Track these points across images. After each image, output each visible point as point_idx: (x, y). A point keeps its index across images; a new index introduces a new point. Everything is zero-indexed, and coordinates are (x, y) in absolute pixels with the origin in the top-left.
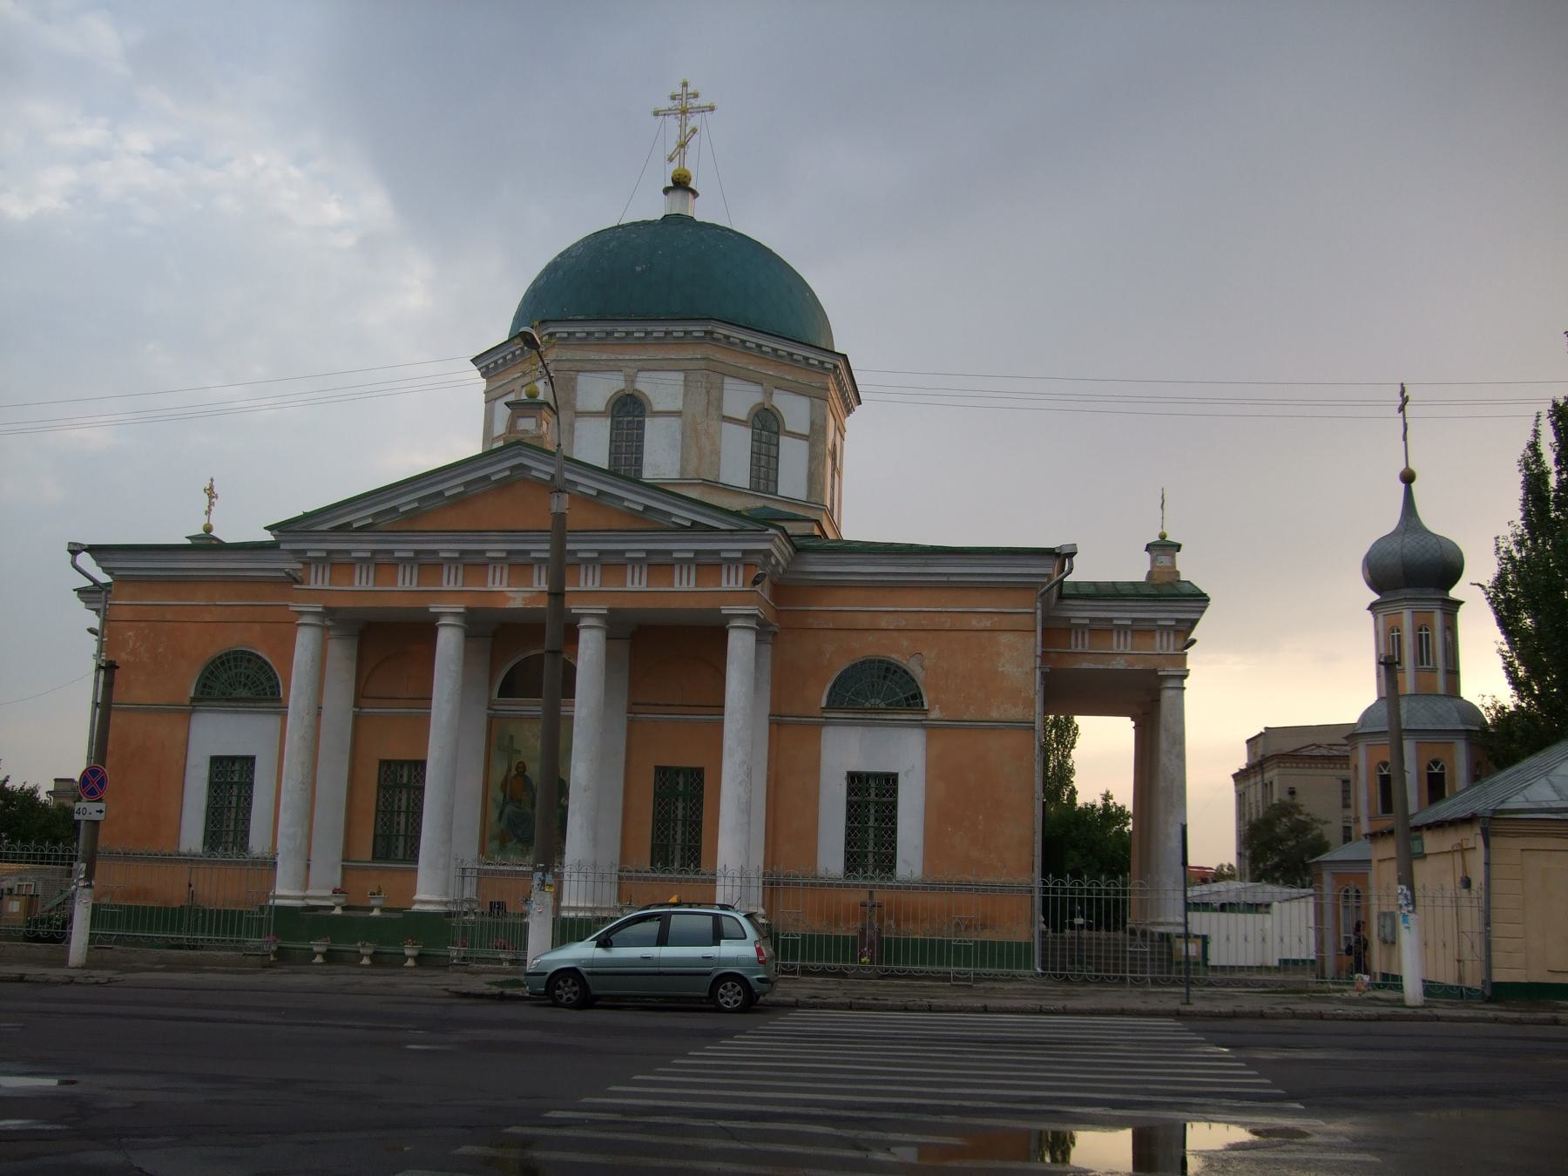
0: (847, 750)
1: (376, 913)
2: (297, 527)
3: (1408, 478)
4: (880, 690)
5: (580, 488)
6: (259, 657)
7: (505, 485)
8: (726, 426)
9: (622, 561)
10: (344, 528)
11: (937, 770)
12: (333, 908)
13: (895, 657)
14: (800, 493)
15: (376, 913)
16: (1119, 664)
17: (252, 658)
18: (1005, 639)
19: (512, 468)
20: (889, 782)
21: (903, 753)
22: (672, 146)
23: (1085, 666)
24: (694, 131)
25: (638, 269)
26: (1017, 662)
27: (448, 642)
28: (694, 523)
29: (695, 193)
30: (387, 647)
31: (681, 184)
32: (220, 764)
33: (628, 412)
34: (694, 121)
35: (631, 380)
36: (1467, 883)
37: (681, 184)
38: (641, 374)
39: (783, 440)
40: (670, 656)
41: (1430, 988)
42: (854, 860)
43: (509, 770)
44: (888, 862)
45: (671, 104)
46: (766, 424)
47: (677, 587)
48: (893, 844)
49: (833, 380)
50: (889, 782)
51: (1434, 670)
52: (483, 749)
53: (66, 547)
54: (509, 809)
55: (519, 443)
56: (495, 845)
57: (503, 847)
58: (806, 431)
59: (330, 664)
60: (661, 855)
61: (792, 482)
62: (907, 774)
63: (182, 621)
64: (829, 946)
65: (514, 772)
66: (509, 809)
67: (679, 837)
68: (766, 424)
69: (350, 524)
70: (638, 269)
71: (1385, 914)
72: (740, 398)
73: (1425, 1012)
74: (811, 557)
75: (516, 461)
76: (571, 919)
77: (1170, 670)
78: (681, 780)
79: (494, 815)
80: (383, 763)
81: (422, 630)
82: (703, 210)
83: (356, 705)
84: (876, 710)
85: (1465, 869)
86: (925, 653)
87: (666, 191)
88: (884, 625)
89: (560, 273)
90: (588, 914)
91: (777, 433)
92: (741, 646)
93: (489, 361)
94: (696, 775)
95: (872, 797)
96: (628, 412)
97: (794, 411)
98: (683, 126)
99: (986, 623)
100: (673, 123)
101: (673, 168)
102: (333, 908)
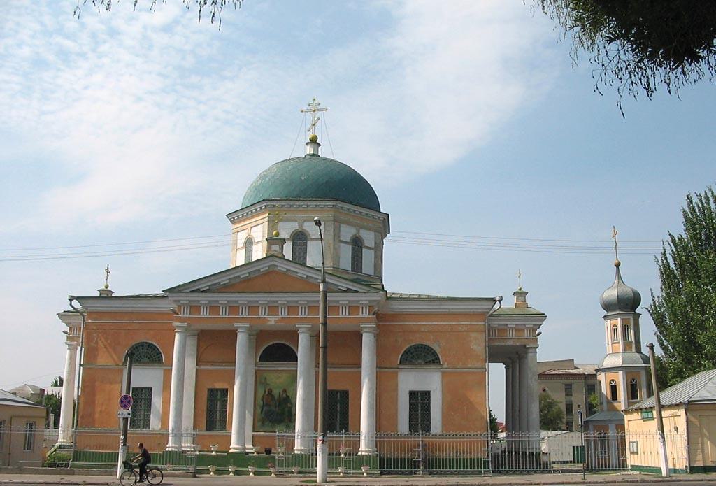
0: (409, 380)
1: (214, 453)
2: (177, 289)
3: (618, 265)
4: (421, 356)
5: (299, 275)
6: (153, 345)
7: (267, 273)
8: (342, 245)
9: (258, 305)
10: (197, 291)
11: (447, 389)
12: (253, 453)
13: (428, 343)
14: (371, 272)
15: (214, 453)
16: (510, 343)
17: (142, 345)
18: (473, 335)
19: (269, 266)
20: (427, 395)
21: (431, 381)
22: (318, 124)
23: (497, 344)
24: (319, 119)
25: (303, 178)
26: (478, 344)
27: (241, 339)
28: (348, 289)
29: (319, 145)
30: (214, 345)
31: (314, 141)
32: (413, 395)
33: (300, 239)
34: (318, 114)
35: (301, 226)
36: (677, 429)
37: (314, 141)
38: (305, 223)
39: (364, 250)
40: (338, 346)
41: (669, 470)
42: (413, 427)
43: (265, 391)
44: (427, 428)
45: (308, 107)
46: (357, 244)
47: (341, 316)
48: (429, 420)
49: (383, 225)
50: (427, 395)
51: (619, 343)
52: (254, 383)
53: (68, 298)
54: (265, 408)
55: (272, 255)
56: (260, 424)
57: (263, 424)
58: (373, 246)
59: (187, 348)
60: (210, 426)
61: (367, 268)
62: (434, 391)
63: (115, 331)
64: (109, 456)
65: (267, 393)
66: (265, 408)
67: (338, 419)
68: (357, 244)
69: (199, 289)
70: (303, 178)
71: (633, 442)
72: (347, 233)
73: (669, 478)
74: (392, 302)
75: (273, 263)
76: (298, 454)
77: (531, 345)
78: (339, 394)
79: (259, 411)
80: (209, 390)
81: (229, 337)
82: (324, 152)
83: (197, 365)
84: (144, 363)
85: (675, 423)
86: (440, 341)
87: (307, 144)
88: (423, 330)
89: (267, 179)
90: (366, 454)
91: (361, 247)
92: (367, 340)
93: (235, 216)
94: (225, 392)
95: (420, 401)
96: (300, 239)
97: (368, 238)
98: (314, 117)
99: (465, 328)
100: (309, 115)
101: (310, 135)
102: (253, 453)
